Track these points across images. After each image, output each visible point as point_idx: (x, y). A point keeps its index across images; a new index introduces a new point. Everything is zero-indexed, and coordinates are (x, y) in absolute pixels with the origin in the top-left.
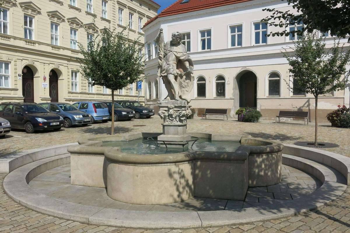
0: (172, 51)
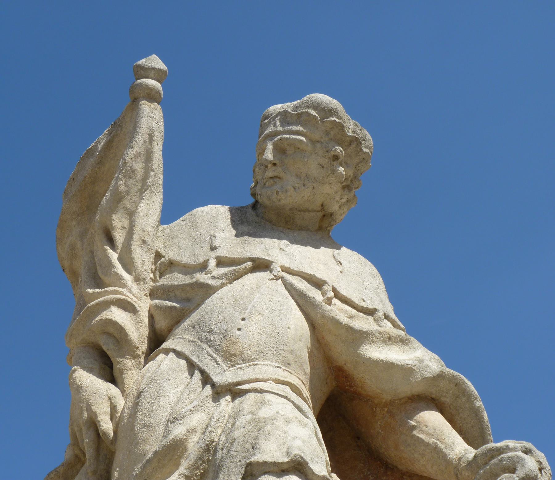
0: (261, 265)
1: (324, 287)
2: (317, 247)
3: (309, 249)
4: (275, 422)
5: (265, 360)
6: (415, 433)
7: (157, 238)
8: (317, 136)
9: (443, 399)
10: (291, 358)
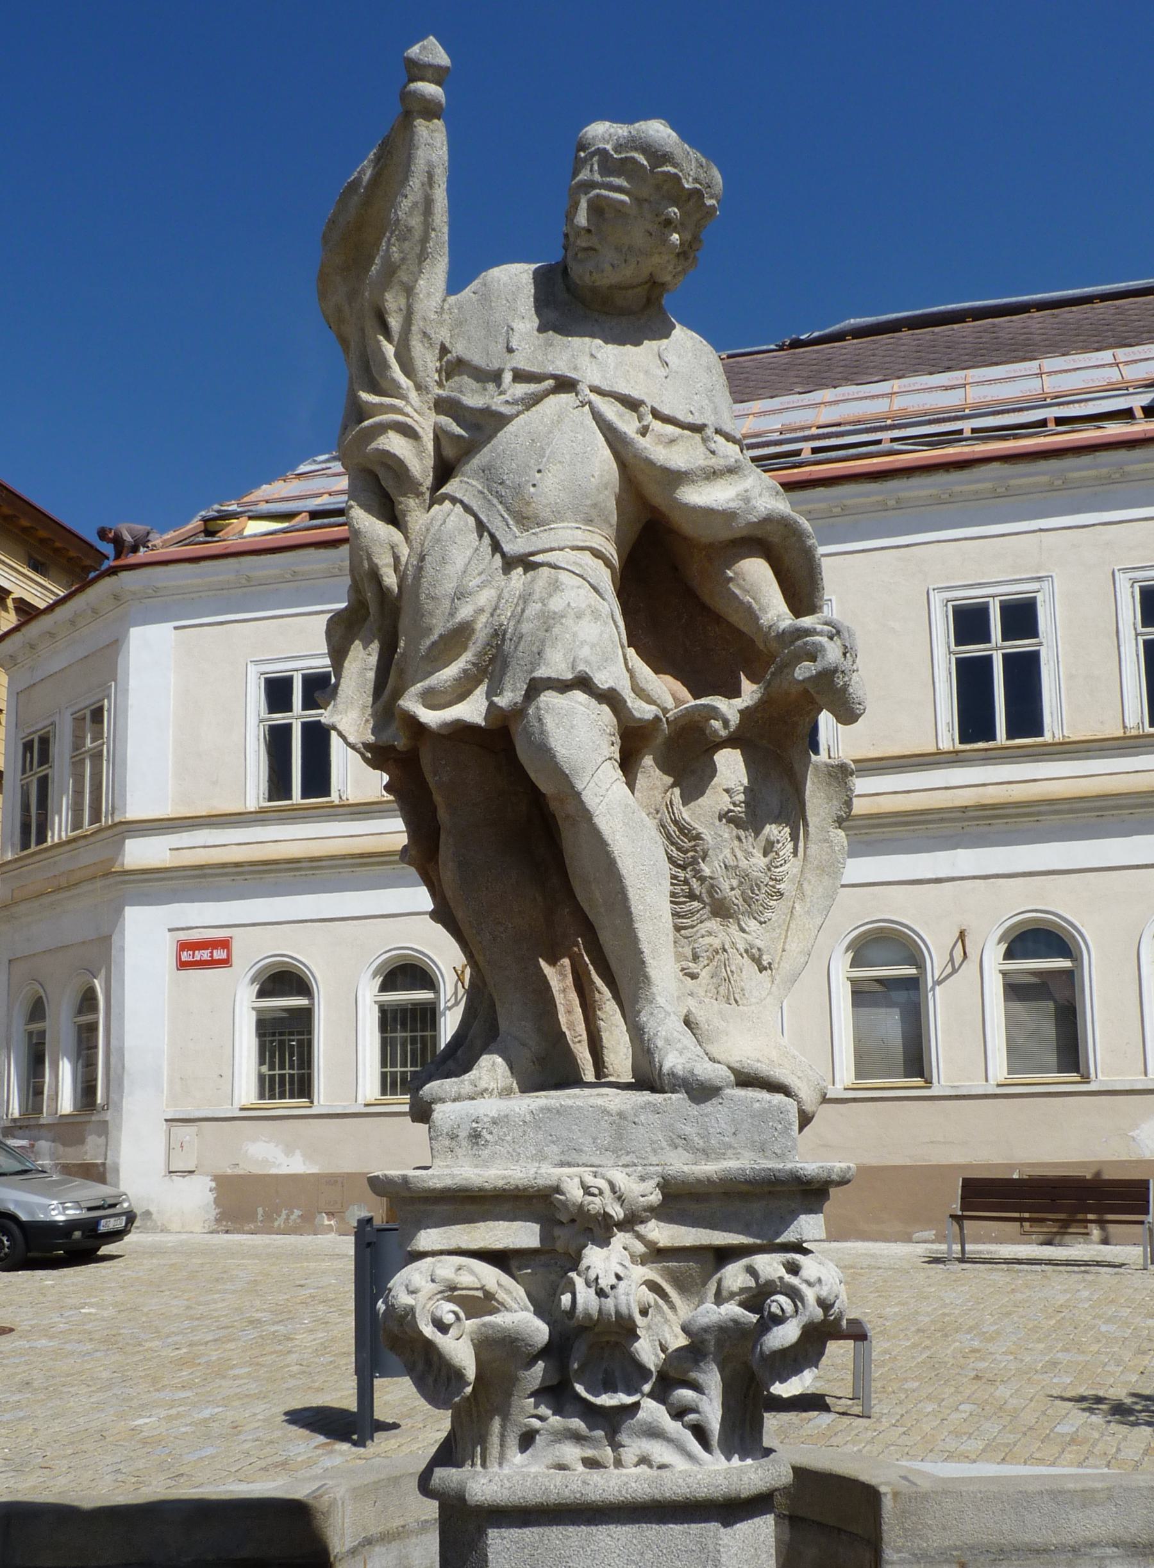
0: (565, 385)
1: (641, 409)
2: (637, 343)
3: (629, 348)
4: (564, 621)
5: (563, 521)
6: (731, 585)
7: (442, 323)
8: (645, 192)
9: (770, 539)
10: (594, 513)
